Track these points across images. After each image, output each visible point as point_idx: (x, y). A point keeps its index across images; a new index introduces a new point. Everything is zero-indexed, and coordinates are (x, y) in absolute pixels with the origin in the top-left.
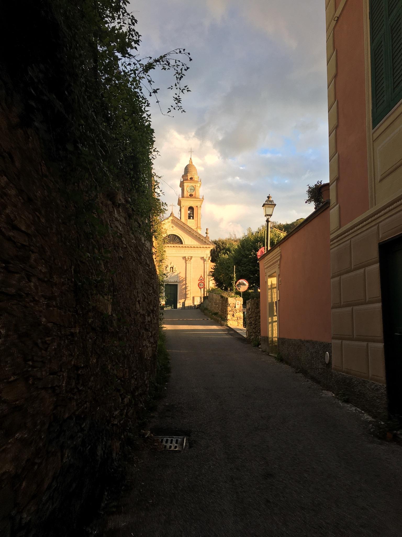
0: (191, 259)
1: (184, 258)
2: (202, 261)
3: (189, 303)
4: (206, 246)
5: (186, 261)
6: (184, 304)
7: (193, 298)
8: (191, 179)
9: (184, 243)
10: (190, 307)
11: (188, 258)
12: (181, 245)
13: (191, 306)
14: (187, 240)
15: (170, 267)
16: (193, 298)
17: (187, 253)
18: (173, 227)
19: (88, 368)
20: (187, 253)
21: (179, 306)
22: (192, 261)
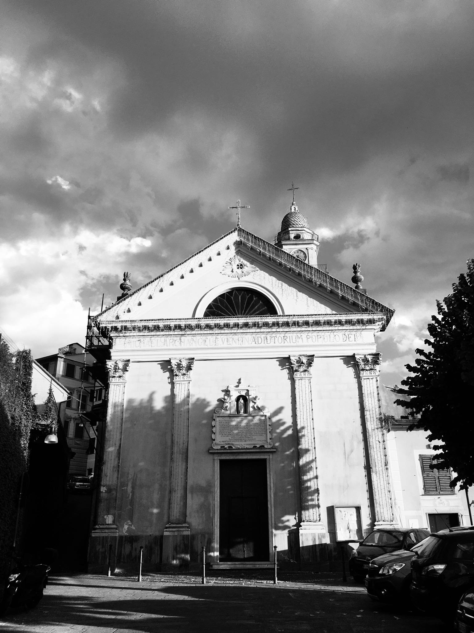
0: (310, 364)
1: (285, 362)
2: (351, 371)
3: (313, 533)
4: (355, 317)
5: (292, 372)
6: (294, 536)
7: (331, 511)
8: (297, 237)
9: (279, 312)
10: (318, 550)
11: (300, 362)
12: (270, 320)
13: (323, 547)
14: (292, 301)
15: (234, 394)
16: (331, 511)
17: (296, 344)
18: (241, 266)
19: (257, 407)
20: (296, 344)
21: (280, 541)
22: (311, 369)
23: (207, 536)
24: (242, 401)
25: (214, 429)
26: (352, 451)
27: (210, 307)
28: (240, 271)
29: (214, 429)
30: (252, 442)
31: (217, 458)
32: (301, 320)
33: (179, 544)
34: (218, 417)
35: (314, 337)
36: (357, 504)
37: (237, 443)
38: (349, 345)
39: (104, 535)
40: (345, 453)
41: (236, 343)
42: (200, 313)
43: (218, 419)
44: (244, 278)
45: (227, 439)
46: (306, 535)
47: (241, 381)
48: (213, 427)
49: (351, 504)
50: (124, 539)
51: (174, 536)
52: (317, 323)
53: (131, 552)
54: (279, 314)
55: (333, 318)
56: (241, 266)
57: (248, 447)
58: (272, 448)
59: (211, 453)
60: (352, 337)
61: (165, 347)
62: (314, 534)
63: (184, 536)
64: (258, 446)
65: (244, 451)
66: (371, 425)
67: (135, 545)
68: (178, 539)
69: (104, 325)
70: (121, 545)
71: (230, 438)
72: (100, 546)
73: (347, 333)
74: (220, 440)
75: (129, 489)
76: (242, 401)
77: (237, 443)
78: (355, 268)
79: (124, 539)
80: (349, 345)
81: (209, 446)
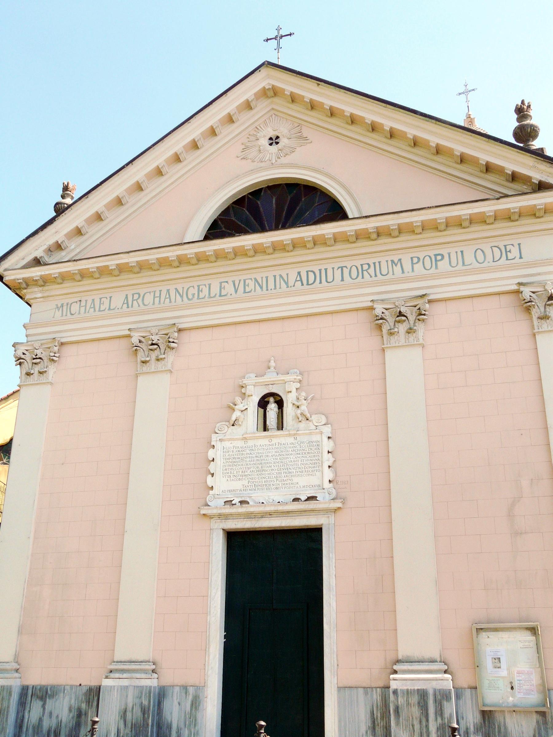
18: (274, 141)
23: (191, 690)
25: (212, 467)
29: (212, 467)
34: (221, 440)
43: (218, 445)
44: (284, 160)
45: (237, 485)
47: (536, 118)
53: (41, 720)
54: (350, 216)
55: (488, 208)
64: (303, 498)
65: (207, 642)
67: (50, 703)
70: (22, 703)
71: (245, 482)
76: (272, 407)
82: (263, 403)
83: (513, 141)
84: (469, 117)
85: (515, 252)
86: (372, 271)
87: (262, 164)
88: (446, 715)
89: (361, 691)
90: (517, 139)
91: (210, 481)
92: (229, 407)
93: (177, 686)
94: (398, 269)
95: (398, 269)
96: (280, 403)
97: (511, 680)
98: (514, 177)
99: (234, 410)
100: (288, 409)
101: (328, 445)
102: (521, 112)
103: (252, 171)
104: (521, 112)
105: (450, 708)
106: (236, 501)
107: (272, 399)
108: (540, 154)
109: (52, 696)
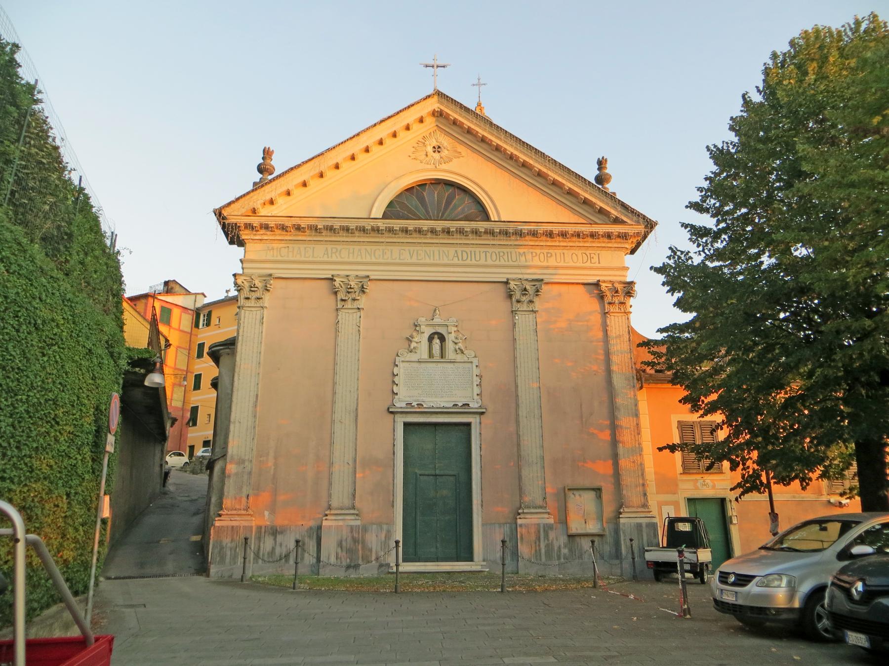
9: (493, 216)
12: (482, 226)
18: (437, 149)
24: (438, 341)
25: (396, 380)
26: (591, 414)
27: (391, 204)
28: (437, 155)
30: (454, 399)
31: (400, 420)
32: (541, 228)
33: (345, 538)
35: (542, 255)
36: (596, 484)
37: (430, 399)
38: (591, 268)
39: (234, 524)
40: (581, 417)
41: (430, 257)
42: (378, 211)
43: (401, 365)
44: (444, 166)
46: (527, 526)
48: (394, 375)
49: (587, 484)
50: (263, 530)
51: (338, 527)
52: (563, 234)
53: (273, 549)
55: (586, 229)
56: (437, 149)
57: (446, 405)
58: (480, 407)
59: (392, 413)
60: (596, 258)
61: (326, 259)
62: (539, 525)
63: (352, 527)
64: (460, 404)
66: (618, 381)
68: (344, 533)
69: (234, 221)
72: (229, 540)
73: (588, 252)
74: (405, 396)
75: (271, 463)
76: (436, 342)
77: (430, 399)
78: (660, 449)
79: (263, 530)
80: (591, 268)
81: (389, 403)
82: (431, 339)
83: (594, 182)
84: (479, 105)
85: (596, 259)
86: (506, 257)
87: (429, 167)
88: (551, 538)
89: (497, 526)
90: (597, 182)
91: (395, 389)
92: (407, 339)
93: (373, 524)
94: (523, 258)
95: (523, 258)
96: (442, 339)
97: (248, 536)
98: (601, 211)
99: (411, 341)
100: (450, 346)
101: (476, 371)
102: (601, 163)
103: (418, 171)
104: (601, 163)
105: (552, 535)
106: (414, 404)
107: (436, 336)
108: (612, 197)
109: (282, 533)
